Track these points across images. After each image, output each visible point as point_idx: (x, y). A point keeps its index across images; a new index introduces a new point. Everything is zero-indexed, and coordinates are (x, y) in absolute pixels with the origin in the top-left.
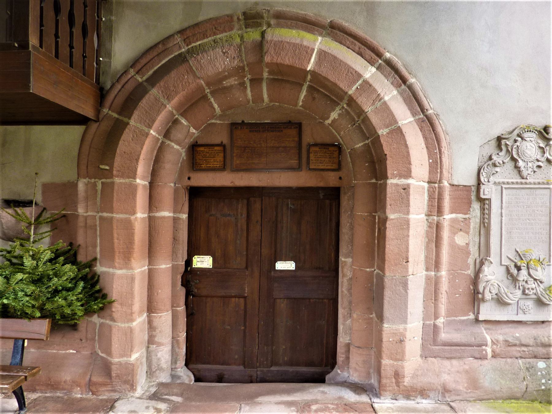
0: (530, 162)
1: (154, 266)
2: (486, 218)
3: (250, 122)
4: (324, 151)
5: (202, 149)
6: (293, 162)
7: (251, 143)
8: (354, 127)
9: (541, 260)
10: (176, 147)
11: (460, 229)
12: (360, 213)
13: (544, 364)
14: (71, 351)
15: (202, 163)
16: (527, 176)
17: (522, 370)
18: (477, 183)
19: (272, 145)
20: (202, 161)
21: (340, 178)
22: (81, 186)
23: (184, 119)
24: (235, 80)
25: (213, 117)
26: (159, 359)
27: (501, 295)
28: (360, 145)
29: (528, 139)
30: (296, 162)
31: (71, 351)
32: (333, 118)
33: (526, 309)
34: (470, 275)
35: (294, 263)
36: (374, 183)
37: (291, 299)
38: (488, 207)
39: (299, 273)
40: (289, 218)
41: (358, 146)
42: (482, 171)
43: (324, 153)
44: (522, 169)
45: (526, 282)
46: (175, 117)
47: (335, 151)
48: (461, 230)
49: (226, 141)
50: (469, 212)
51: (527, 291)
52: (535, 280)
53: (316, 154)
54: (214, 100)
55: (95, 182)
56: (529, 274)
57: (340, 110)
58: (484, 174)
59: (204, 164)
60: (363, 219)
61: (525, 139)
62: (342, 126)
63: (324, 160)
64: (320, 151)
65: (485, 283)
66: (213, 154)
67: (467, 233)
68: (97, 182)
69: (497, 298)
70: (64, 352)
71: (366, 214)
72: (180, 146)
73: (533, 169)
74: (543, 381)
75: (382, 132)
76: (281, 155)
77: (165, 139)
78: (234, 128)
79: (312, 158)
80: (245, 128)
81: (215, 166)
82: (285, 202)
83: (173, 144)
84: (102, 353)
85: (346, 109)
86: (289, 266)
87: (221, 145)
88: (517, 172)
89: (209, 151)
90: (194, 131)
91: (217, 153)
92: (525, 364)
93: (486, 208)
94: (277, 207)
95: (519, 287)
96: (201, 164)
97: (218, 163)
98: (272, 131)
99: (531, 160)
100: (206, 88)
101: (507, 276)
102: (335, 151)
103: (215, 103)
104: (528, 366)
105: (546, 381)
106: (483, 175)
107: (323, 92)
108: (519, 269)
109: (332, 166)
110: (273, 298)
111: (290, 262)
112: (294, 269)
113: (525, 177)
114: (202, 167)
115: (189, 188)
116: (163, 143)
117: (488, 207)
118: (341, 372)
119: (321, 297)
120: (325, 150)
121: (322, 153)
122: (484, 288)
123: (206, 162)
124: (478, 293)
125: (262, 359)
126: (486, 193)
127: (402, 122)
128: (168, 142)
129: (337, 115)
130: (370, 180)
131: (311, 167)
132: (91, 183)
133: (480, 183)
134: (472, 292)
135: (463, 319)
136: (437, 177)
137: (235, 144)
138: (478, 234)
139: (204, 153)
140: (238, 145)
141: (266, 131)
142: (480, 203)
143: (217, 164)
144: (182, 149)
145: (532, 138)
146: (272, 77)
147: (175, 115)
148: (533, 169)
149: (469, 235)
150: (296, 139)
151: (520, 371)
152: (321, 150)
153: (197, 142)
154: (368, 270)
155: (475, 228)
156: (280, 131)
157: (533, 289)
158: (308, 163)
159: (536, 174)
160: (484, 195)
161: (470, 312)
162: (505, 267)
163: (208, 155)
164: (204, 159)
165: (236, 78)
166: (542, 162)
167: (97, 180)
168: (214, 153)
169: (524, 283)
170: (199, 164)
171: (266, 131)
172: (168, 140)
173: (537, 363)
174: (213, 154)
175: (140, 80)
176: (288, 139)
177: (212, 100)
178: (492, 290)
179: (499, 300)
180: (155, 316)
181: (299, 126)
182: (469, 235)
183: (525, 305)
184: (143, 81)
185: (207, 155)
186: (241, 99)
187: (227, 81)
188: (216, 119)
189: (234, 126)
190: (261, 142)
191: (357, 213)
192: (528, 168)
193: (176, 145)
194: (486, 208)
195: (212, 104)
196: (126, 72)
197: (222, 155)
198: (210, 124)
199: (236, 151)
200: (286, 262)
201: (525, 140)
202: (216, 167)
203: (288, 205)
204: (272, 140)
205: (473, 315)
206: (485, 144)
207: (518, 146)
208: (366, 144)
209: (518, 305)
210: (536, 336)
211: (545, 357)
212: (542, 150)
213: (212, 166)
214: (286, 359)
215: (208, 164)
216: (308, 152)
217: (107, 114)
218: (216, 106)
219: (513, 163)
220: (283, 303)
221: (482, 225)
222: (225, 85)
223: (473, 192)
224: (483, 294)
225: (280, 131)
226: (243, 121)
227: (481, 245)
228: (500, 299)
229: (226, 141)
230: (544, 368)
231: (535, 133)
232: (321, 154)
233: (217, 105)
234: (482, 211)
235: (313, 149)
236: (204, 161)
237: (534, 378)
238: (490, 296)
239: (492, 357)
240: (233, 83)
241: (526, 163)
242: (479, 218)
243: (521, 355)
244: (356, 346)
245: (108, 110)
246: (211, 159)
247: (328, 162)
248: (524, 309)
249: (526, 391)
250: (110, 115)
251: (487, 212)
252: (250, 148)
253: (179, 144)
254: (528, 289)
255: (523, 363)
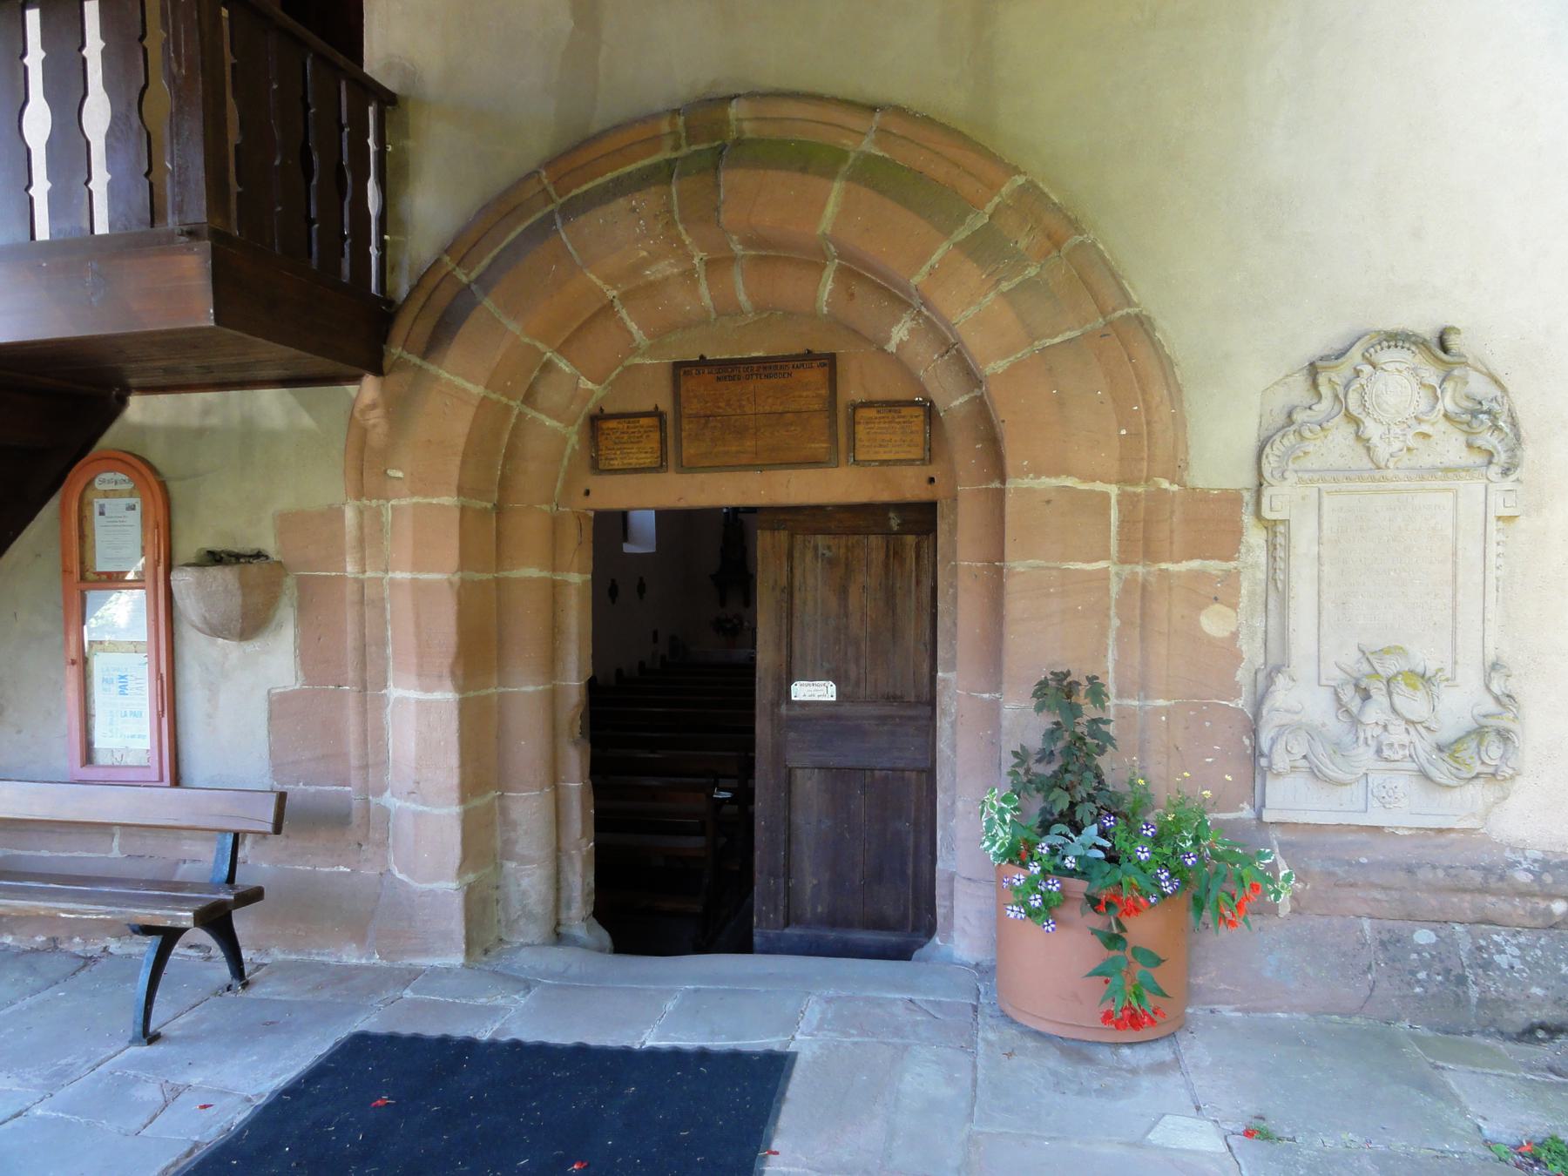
0: (1395, 424)
1: (509, 687)
2: (1280, 569)
3: (718, 357)
4: (888, 417)
5: (613, 424)
6: (817, 445)
7: (721, 404)
8: (946, 358)
9: (1428, 675)
10: (549, 422)
11: (1213, 597)
12: (966, 563)
13: (1432, 934)
14: (342, 869)
15: (613, 456)
16: (1388, 460)
17: (1367, 946)
18: (1257, 483)
19: (767, 409)
20: (613, 452)
21: (932, 480)
22: (350, 515)
23: (564, 361)
24: (671, 265)
25: (634, 351)
26: (524, 893)
27: (1315, 760)
28: (961, 400)
29: (1391, 367)
30: (824, 445)
31: (342, 869)
32: (898, 339)
33: (1390, 797)
34: (1242, 710)
35: (834, 686)
36: (997, 488)
37: (829, 769)
38: (1283, 543)
39: (846, 709)
40: (819, 579)
41: (957, 403)
42: (1268, 449)
43: (890, 422)
44: (1375, 440)
45: (1385, 727)
46: (545, 359)
47: (916, 417)
48: (1216, 599)
49: (665, 405)
50: (1237, 555)
51: (1387, 753)
52: (1409, 722)
53: (869, 426)
54: (629, 315)
55: (378, 506)
56: (1394, 710)
57: (913, 319)
58: (1271, 458)
59: (616, 459)
60: (974, 577)
61: (1384, 366)
62: (919, 358)
63: (888, 439)
64: (880, 418)
65: (1277, 729)
66: (636, 435)
67: (1234, 606)
68: (384, 505)
69: (1310, 768)
70: (327, 870)
71: (979, 564)
72: (560, 421)
73: (1405, 441)
74: (1422, 975)
75: (994, 369)
76: (787, 431)
77: (524, 406)
78: (682, 373)
79: (859, 437)
80: (706, 371)
81: (642, 461)
82: (809, 542)
83: (543, 417)
84: (400, 872)
85: (927, 317)
86: (821, 693)
87: (657, 414)
88: (1364, 451)
89: (628, 427)
90: (590, 385)
91: (645, 432)
92: (1380, 933)
93: (1281, 545)
94: (790, 557)
95: (1366, 739)
96: (612, 459)
97: (648, 455)
98: (767, 376)
99: (1400, 419)
100: (605, 287)
101: (1337, 713)
102: (916, 417)
103: (632, 321)
104: (1385, 937)
105: (1428, 975)
106: (1269, 463)
107: (873, 281)
108: (1366, 696)
109: (909, 452)
110: (786, 766)
111: (823, 682)
112: (834, 699)
113: (1383, 464)
114: (614, 465)
115: (592, 514)
116: (521, 415)
117: (1283, 543)
118: (941, 942)
119: (901, 764)
120: (890, 415)
121: (885, 423)
122: (1274, 741)
123: (621, 453)
124: (1262, 755)
125: (764, 908)
126: (1277, 504)
127: (1044, 341)
128: (531, 413)
129: (906, 332)
130: (988, 484)
131: (860, 457)
132: (371, 507)
133: (1263, 480)
134: (1249, 752)
135: (1225, 818)
136: (1141, 471)
137: (686, 410)
138: (1261, 608)
139: (618, 434)
140: (691, 412)
141: (755, 377)
142: (1265, 532)
143: (647, 458)
144: (567, 426)
145: (1403, 365)
146: (753, 253)
147: (545, 353)
148: (1405, 441)
149: (1237, 613)
150: (824, 392)
151: (1363, 948)
152: (883, 415)
153: (602, 410)
154: (986, 696)
155: (1252, 594)
156: (786, 376)
157: (1403, 746)
158: (852, 448)
159: (1416, 455)
160: (1271, 509)
161: (1242, 803)
162: (1333, 689)
163: (626, 438)
164: (619, 447)
165: (672, 261)
166: (1433, 424)
167: (381, 502)
168: (640, 432)
169: (1378, 731)
170: (606, 459)
171: (755, 377)
172: (532, 408)
173: (1413, 932)
174: (636, 435)
175: (464, 279)
176: (805, 394)
177: (624, 313)
178: (1292, 748)
179: (1313, 771)
180: (513, 797)
181: (829, 362)
182: (1237, 613)
183: (1384, 787)
184: (470, 282)
185: (623, 438)
186: (688, 308)
187: (654, 268)
188: (643, 355)
189: (680, 369)
190: (744, 403)
191: (962, 563)
192: (1392, 439)
193: (548, 419)
194: (1281, 545)
195: (625, 324)
196: (437, 262)
197: (656, 436)
198: (628, 369)
199: (687, 427)
200: (814, 682)
201: (1382, 369)
202: (645, 463)
203: (816, 548)
204: (768, 398)
205: (1252, 811)
206: (1276, 383)
207: (1362, 386)
208: (976, 397)
209: (1367, 786)
210: (1010, 770)
211: (1436, 918)
212: (1430, 392)
213: (634, 461)
214: (819, 909)
215: (625, 458)
216: (852, 423)
217: (400, 358)
218: (633, 327)
219: (1351, 428)
220: (810, 779)
221: (1271, 587)
222: (652, 278)
223: (1247, 504)
224: (1269, 757)
225: (786, 376)
226: (702, 357)
227: (1270, 635)
228: (1316, 771)
229: (665, 405)
230: (1428, 945)
231: (1409, 349)
232: (882, 425)
233: (636, 324)
234: (1270, 552)
235: (864, 414)
236: (618, 452)
237: (1398, 965)
238: (1287, 761)
239: (1293, 911)
240: (668, 273)
241: (1386, 427)
242: (1264, 568)
243: (1368, 911)
244: (964, 875)
245: (400, 349)
246: (630, 446)
247: (898, 443)
248: (1384, 797)
249: (1370, 996)
250: (405, 359)
251: (1282, 555)
252: (719, 418)
253: (557, 417)
254: (1391, 745)
255: (1372, 929)
